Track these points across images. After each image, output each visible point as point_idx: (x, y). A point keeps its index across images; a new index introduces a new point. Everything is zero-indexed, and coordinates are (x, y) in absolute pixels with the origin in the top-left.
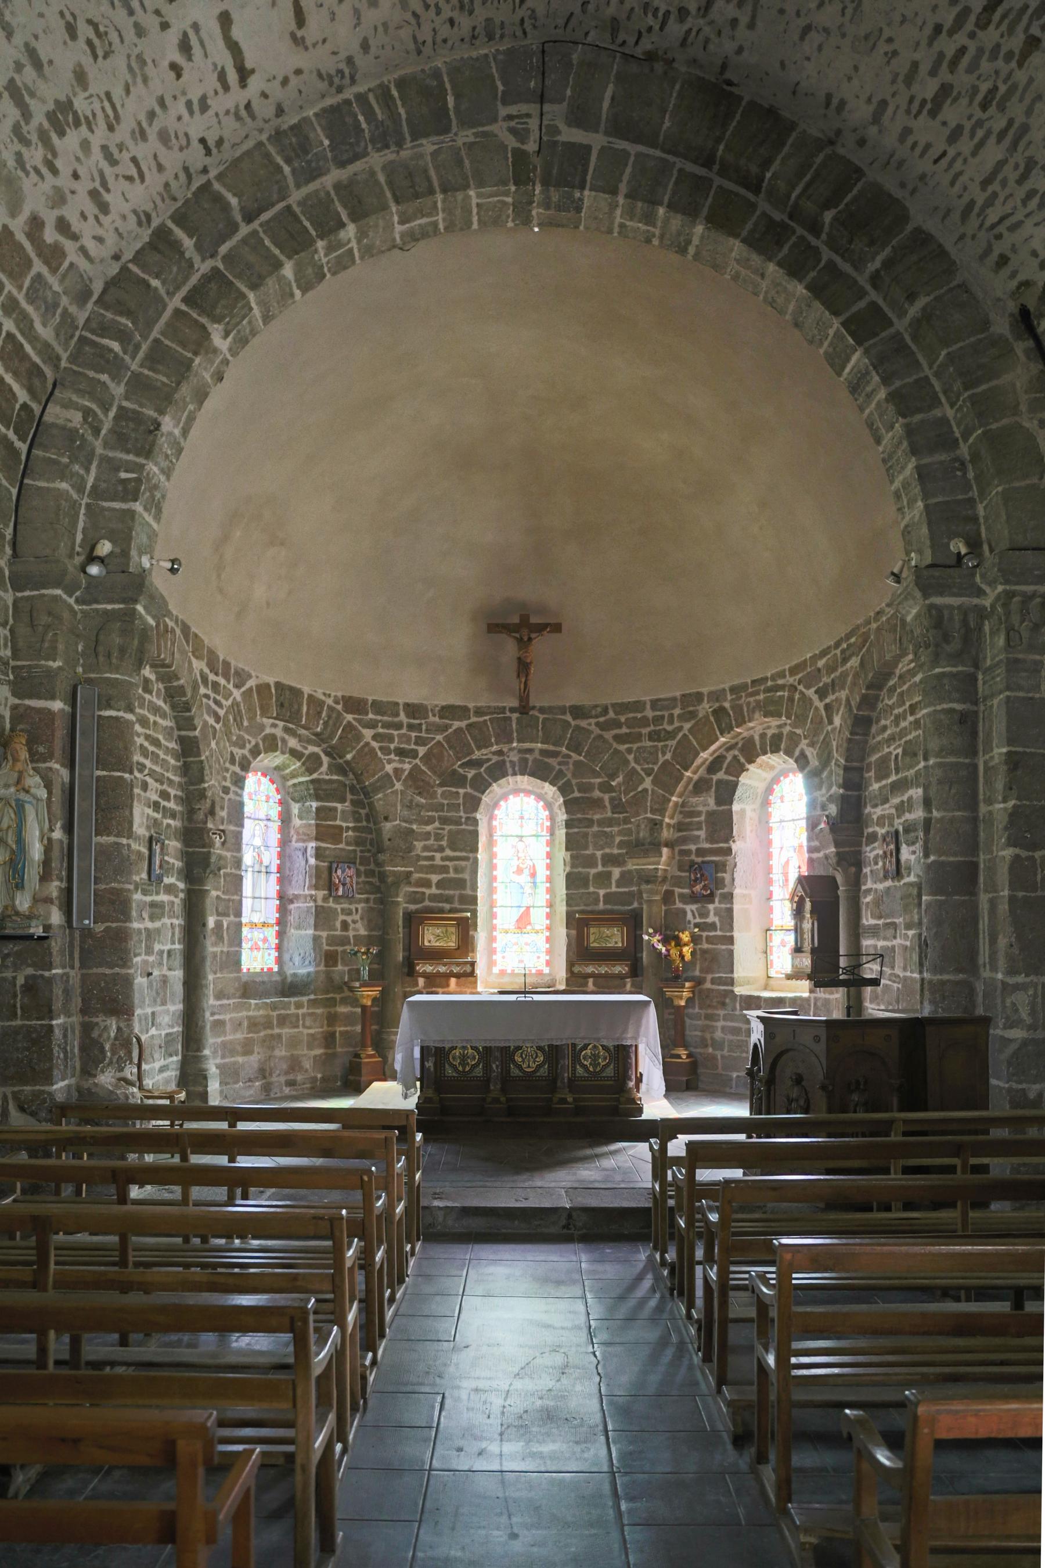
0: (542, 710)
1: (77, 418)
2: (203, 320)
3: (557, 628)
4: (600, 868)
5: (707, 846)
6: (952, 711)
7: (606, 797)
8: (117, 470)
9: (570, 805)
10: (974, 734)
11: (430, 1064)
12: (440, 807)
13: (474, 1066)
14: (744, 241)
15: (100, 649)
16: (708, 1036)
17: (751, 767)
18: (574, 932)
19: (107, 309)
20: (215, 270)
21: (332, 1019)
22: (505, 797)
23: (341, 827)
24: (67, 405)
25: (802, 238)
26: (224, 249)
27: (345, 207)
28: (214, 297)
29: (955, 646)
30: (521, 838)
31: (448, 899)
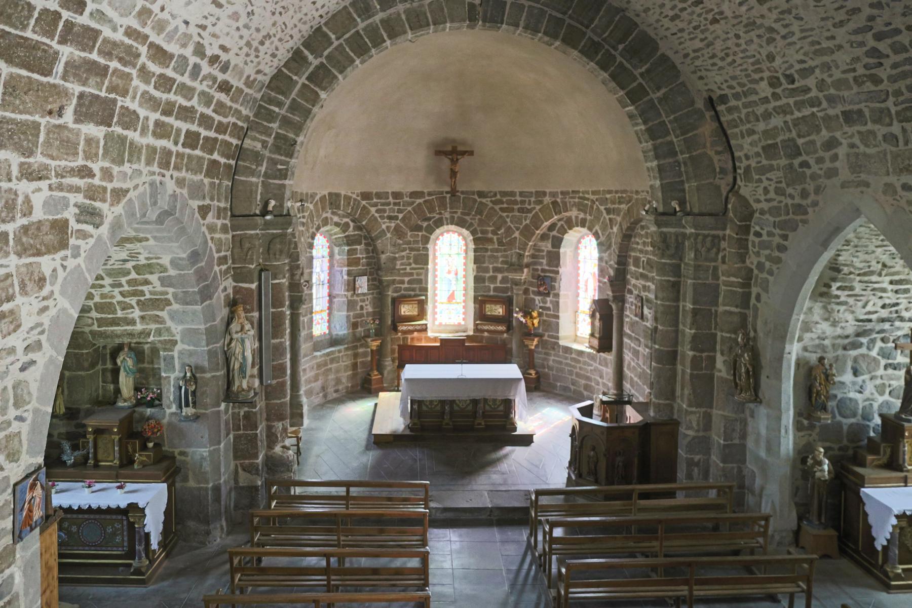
0: (462, 193)
1: (259, 146)
2: (317, 89)
3: (471, 153)
4: (491, 274)
5: (547, 268)
6: (669, 281)
7: (495, 238)
8: (276, 164)
9: (476, 241)
10: (679, 292)
11: (415, 407)
12: (409, 243)
13: (436, 406)
14: (580, 51)
15: (271, 252)
16: (545, 363)
17: (570, 232)
18: (477, 306)
19: (272, 90)
20: (322, 63)
21: (356, 356)
22: (442, 234)
23: (359, 258)
24: (254, 139)
25: (608, 50)
26: (326, 53)
27: (386, 32)
28: (322, 78)
29: (672, 251)
31: (414, 290)
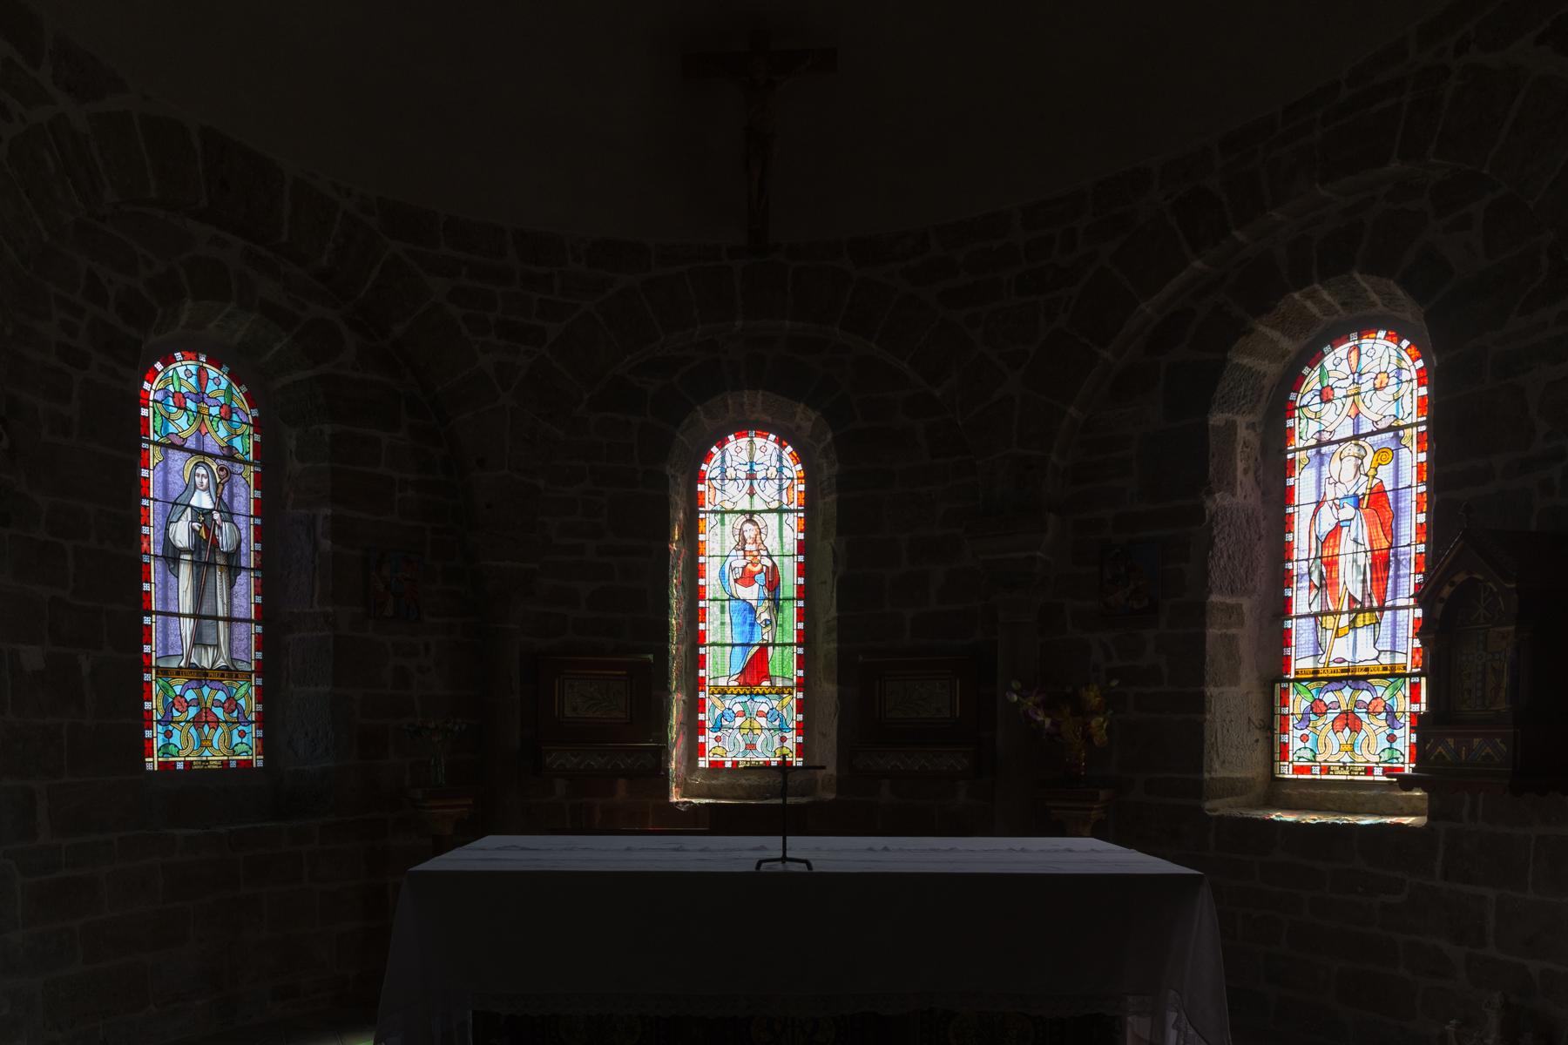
30: (750, 515)
